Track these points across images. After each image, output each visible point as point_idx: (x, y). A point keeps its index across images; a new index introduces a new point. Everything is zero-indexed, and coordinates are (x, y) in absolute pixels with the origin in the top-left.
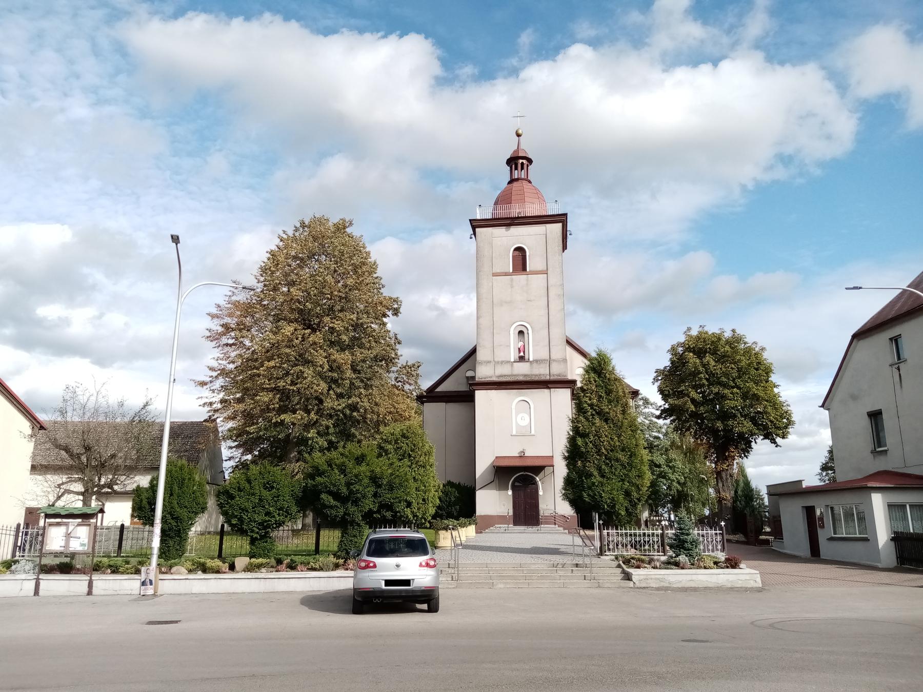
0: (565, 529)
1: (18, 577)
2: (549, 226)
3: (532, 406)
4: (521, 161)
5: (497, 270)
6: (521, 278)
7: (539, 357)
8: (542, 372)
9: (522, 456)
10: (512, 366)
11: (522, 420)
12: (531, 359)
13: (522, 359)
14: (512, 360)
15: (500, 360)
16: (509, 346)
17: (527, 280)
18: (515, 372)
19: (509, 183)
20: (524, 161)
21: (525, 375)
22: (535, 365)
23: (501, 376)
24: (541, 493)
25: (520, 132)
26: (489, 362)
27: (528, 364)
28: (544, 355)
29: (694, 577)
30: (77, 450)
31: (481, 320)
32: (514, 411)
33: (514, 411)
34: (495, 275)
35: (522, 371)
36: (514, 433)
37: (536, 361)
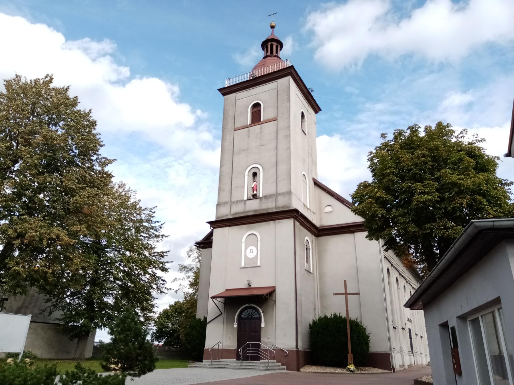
0: (283, 365)
1: (262, 361)
2: (280, 81)
3: (259, 238)
4: (270, 43)
5: (238, 125)
6: (257, 128)
7: (267, 193)
8: (270, 206)
9: (249, 288)
10: (245, 203)
11: (252, 252)
12: (261, 196)
13: (255, 196)
14: (246, 198)
16: (244, 187)
18: (248, 209)
20: (275, 44)
22: (264, 200)
23: (236, 214)
24: (263, 326)
25: (273, 24)
26: (226, 203)
27: (258, 200)
28: (272, 190)
31: (223, 168)
32: (243, 244)
33: (243, 244)
34: (236, 130)
35: (253, 206)
36: (243, 265)
37: (265, 197)
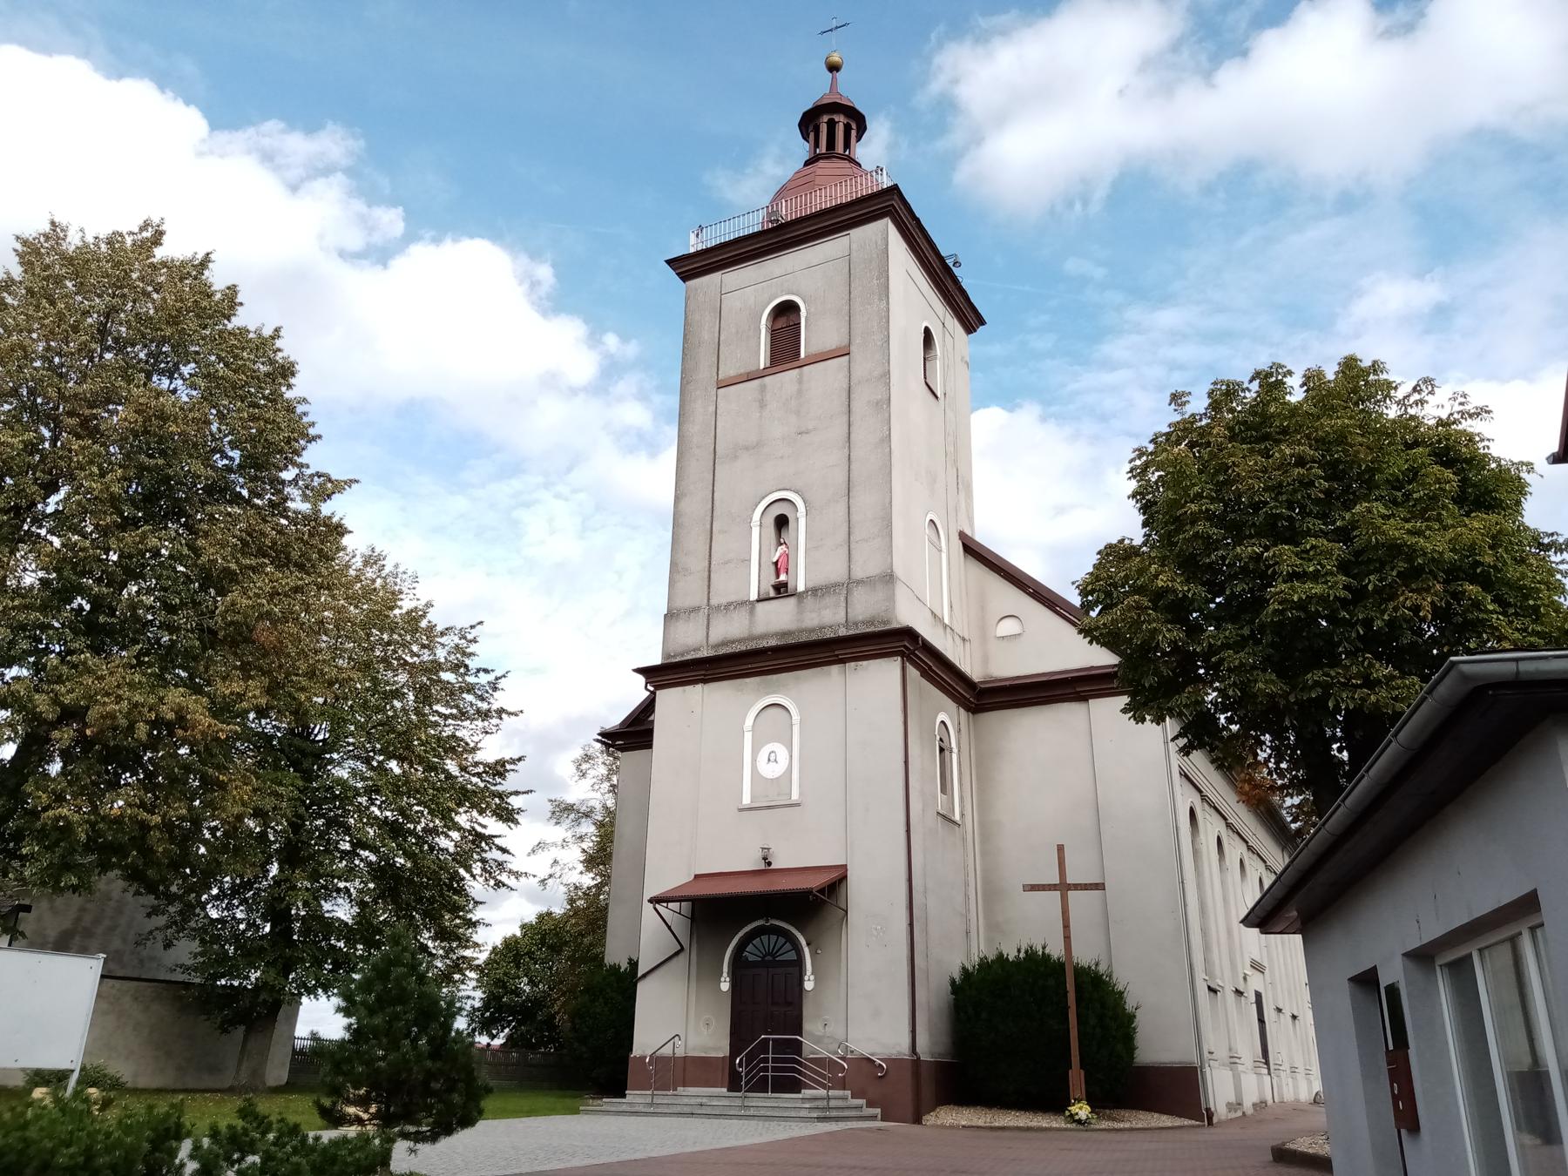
0: (870, 1104)
3: (796, 717)
4: (825, 118)
5: (728, 371)
7: (820, 579)
8: (828, 618)
9: (767, 870)
10: (752, 612)
11: (774, 762)
12: (801, 588)
13: (781, 590)
14: (754, 596)
15: (724, 601)
17: (800, 381)
18: (760, 629)
19: (807, 163)
20: (841, 119)
21: (784, 634)
22: (809, 601)
23: (724, 644)
24: (809, 985)
25: (836, 58)
26: (696, 609)
27: (792, 601)
28: (833, 571)
29: (1524, 667)
30: (474, 633)
31: (683, 505)
32: (748, 737)
33: (748, 737)
35: (778, 620)
36: (746, 800)
37: (814, 591)
